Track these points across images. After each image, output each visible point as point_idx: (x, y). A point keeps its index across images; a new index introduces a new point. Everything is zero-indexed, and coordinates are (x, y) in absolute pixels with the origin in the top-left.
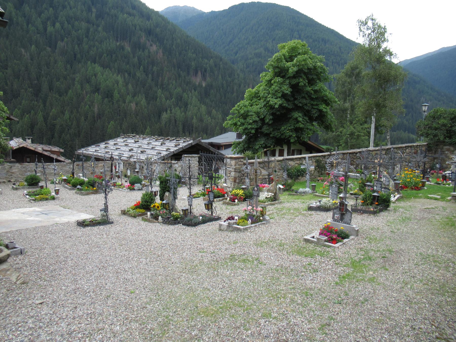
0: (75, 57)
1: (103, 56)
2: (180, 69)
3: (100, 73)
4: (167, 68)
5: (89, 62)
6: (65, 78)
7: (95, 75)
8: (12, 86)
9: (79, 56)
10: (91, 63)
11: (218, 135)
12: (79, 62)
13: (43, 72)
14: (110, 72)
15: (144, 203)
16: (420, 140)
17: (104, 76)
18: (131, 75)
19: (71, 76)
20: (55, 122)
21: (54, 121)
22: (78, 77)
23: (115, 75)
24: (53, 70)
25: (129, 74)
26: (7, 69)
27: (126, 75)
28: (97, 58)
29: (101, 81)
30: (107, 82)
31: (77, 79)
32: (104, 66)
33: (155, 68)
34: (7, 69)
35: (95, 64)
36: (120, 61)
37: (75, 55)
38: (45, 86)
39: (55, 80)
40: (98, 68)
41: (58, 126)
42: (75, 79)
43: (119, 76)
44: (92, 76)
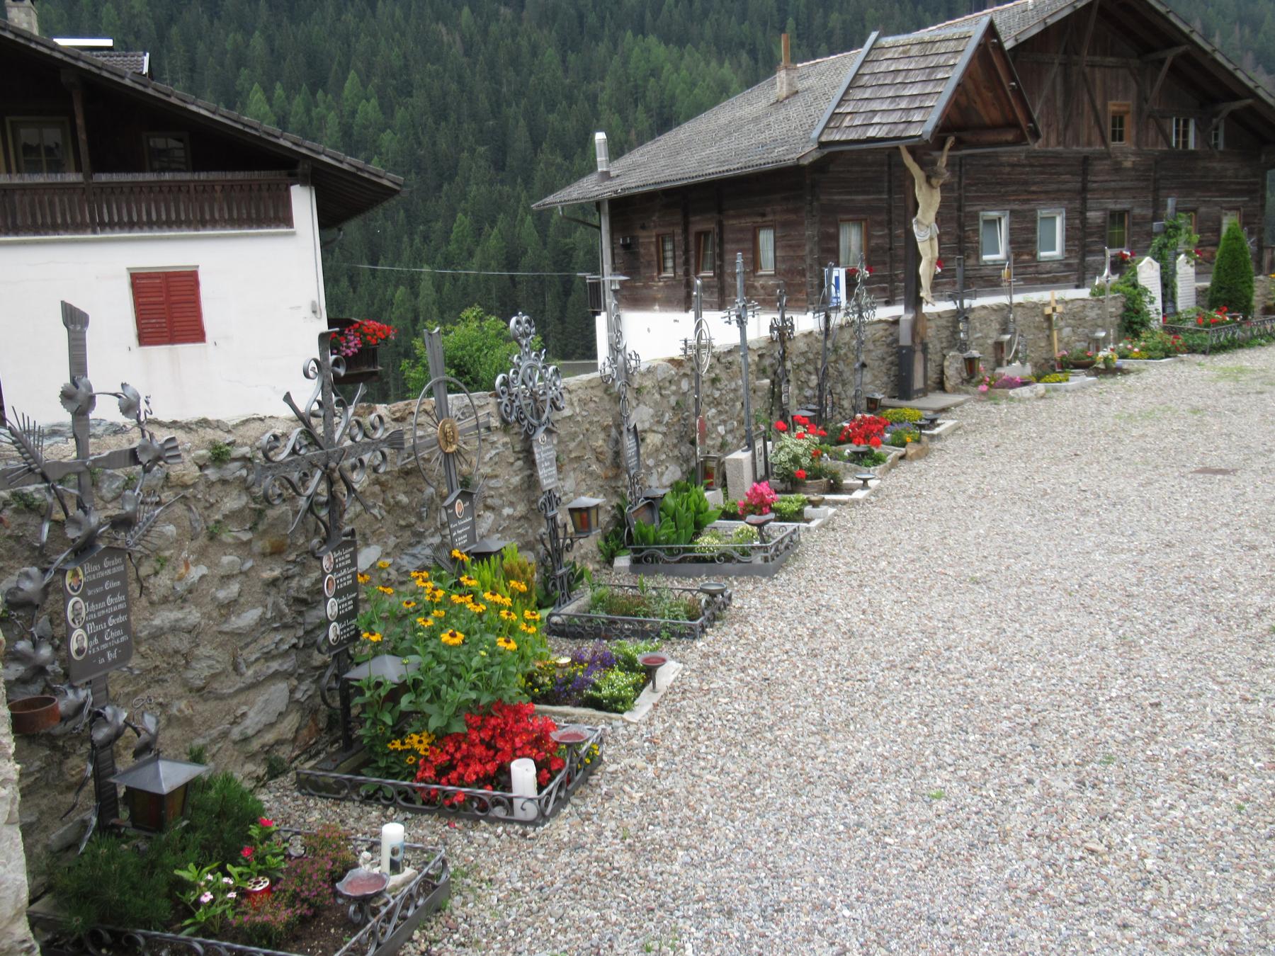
0: (581, 24)
1: (665, 8)
2: (920, 8)
3: (668, 66)
4: (876, 9)
5: (629, 33)
6: (571, 100)
7: (655, 73)
8: (434, 144)
9: (592, 19)
10: (635, 35)
11: (563, 187)
12: (597, 38)
13: (504, 89)
14: (697, 55)
15: (41, 879)
16: (837, 298)
17: (684, 73)
18: (760, 56)
19: (584, 88)
20: (568, 240)
21: (565, 237)
22: (606, 89)
23: (714, 64)
24: (533, 78)
25: (753, 53)
26: (410, 95)
27: (744, 57)
28: (648, 15)
29: (678, 91)
30: (696, 91)
31: (604, 97)
32: (672, 38)
33: (835, 16)
34: (410, 95)
35: (645, 36)
36: (719, 13)
37: (581, 17)
38: (520, 137)
39: (542, 108)
40: (659, 51)
41: (581, 254)
42: (595, 97)
43: (727, 64)
44: (646, 80)
